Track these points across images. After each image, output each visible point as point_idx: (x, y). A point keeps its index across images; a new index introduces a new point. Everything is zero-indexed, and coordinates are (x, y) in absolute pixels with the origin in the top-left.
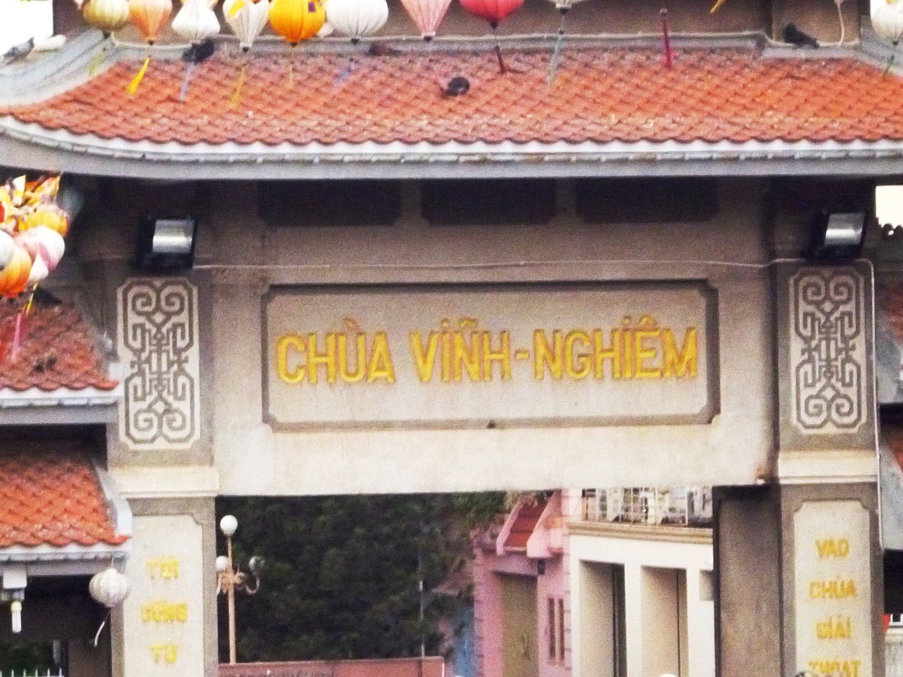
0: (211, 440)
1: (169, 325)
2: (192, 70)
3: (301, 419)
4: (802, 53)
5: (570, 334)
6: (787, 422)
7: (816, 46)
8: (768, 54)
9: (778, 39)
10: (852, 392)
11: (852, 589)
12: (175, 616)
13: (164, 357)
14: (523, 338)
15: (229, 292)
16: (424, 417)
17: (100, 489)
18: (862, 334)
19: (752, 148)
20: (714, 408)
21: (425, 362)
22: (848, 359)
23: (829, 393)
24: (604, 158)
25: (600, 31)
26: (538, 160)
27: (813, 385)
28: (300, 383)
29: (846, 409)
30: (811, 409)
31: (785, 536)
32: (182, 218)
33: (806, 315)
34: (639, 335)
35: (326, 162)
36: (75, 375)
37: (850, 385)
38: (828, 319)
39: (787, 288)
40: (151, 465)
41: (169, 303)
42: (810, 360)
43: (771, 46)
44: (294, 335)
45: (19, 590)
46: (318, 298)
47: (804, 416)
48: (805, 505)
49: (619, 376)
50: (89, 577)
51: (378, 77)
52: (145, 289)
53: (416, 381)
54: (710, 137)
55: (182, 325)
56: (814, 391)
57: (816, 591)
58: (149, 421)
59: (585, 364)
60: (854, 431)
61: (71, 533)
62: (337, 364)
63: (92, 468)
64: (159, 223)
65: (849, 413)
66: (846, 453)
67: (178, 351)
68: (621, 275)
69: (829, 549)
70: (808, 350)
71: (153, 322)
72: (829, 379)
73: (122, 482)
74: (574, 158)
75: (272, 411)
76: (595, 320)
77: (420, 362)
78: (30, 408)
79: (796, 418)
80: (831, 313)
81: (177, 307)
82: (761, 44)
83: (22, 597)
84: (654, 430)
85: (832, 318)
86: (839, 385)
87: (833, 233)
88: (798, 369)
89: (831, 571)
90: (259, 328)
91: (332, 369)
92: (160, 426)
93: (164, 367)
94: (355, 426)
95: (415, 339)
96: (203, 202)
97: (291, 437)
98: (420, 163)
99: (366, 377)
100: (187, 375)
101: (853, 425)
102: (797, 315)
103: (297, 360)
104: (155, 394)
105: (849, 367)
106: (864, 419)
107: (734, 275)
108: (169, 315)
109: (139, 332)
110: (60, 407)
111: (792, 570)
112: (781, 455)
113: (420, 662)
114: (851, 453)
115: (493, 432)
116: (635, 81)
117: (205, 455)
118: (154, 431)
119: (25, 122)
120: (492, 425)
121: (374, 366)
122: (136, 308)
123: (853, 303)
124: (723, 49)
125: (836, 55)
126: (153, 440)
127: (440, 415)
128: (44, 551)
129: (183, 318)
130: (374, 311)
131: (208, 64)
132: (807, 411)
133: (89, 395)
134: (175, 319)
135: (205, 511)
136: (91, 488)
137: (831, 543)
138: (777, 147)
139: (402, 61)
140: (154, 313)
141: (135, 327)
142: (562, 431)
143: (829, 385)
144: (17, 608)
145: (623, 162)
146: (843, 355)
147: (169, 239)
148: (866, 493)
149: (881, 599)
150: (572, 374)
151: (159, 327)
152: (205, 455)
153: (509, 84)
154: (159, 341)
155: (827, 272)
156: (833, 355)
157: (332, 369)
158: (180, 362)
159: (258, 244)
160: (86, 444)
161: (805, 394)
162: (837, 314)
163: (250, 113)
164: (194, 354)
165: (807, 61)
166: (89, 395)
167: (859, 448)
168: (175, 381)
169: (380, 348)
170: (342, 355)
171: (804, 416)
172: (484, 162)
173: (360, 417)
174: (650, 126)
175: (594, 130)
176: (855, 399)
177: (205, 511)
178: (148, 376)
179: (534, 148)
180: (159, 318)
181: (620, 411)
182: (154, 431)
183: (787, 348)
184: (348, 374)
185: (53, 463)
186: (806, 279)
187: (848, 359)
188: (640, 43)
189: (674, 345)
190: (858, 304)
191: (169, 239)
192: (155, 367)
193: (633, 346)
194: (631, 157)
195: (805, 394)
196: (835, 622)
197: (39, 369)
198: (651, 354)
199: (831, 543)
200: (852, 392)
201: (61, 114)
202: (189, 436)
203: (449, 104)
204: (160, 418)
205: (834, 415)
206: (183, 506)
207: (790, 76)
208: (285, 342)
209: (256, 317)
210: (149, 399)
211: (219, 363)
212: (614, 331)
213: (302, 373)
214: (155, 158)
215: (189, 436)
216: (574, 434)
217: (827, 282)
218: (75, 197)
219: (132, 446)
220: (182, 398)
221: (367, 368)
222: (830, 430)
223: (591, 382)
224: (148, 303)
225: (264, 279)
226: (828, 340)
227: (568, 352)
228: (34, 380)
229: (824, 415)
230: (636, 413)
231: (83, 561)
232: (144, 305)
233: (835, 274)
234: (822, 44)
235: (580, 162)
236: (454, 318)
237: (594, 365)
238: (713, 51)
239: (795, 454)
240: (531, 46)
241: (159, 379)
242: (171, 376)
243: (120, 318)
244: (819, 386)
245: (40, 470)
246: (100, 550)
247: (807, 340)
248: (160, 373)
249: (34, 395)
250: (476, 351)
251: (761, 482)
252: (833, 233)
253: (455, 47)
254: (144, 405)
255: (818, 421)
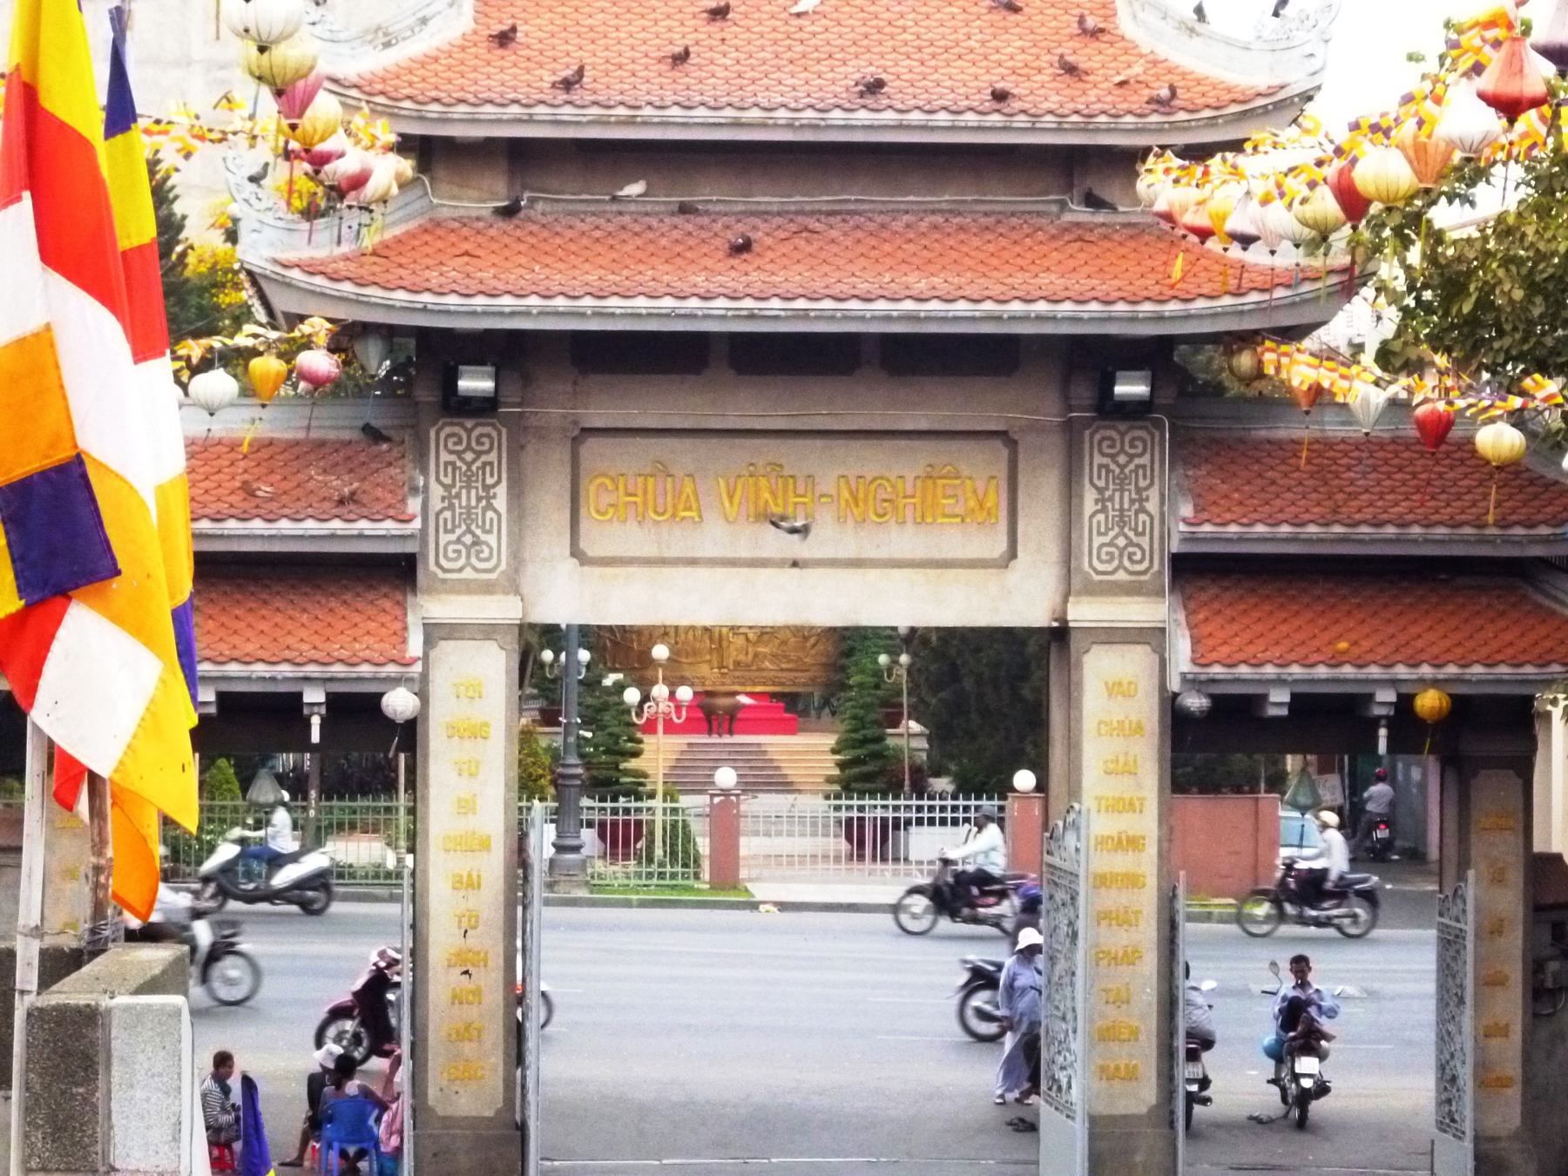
0: (517, 571)
1: (478, 464)
2: (501, 224)
3: (630, 554)
4: (1100, 217)
5: (875, 479)
6: (1080, 569)
7: (1112, 208)
8: (1068, 217)
9: (1079, 204)
10: (1145, 542)
11: (1140, 727)
12: (477, 733)
13: (473, 492)
14: (827, 484)
15: (542, 434)
16: (730, 554)
17: (405, 614)
18: (1156, 486)
19: (1016, 307)
20: (1012, 553)
21: (731, 503)
22: (490, 506)
23: (1121, 542)
24: (868, 315)
25: (907, 195)
26: (804, 315)
27: (1105, 534)
28: (610, 521)
29: (1138, 557)
30: (1104, 557)
31: (1074, 678)
32: (483, 363)
33: (1100, 466)
34: (940, 482)
35: (598, 314)
36: (378, 507)
37: (1143, 534)
38: (469, 469)
39: (1082, 442)
40: (458, 592)
41: (479, 443)
42: (1104, 510)
43: (1071, 210)
44: (604, 475)
45: (319, 704)
46: (629, 440)
47: (1095, 562)
48: (1095, 647)
49: (921, 521)
50: (381, 695)
51: (676, 234)
52: (456, 429)
53: (722, 521)
54: (975, 297)
55: (491, 464)
56: (1106, 539)
57: (1104, 729)
58: (458, 552)
59: (888, 510)
60: (1143, 578)
61: (367, 654)
62: (645, 504)
63: (405, 595)
64: (462, 368)
65: (1141, 562)
66: (1136, 599)
67: (486, 488)
68: (923, 425)
69: (1116, 689)
70: (1101, 500)
71: (462, 460)
72: (1122, 528)
73: (430, 607)
74: (839, 314)
75: (582, 545)
76: (900, 468)
77: (727, 504)
78: (332, 537)
79: (1092, 564)
80: (1126, 466)
81: (486, 447)
82: (1063, 205)
83: (323, 710)
84: (951, 573)
85: (1127, 471)
86: (1131, 534)
87: (1120, 389)
88: (1091, 517)
89: (1119, 711)
90: (569, 469)
91: (640, 509)
92: (468, 557)
93: (473, 503)
94: (663, 562)
95: (722, 482)
96: (511, 350)
97: (597, 571)
98: (691, 316)
99: (674, 516)
100: (496, 511)
101: (1144, 572)
102: (437, 465)
103: (607, 499)
104: (464, 527)
105: (490, 514)
106: (1156, 567)
107: (1035, 428)
108: (479, 454)
109: (450, 469)
110: (361, 536)
111: (1080, 709)
112: (1071, 599)
113: (1257, 799)
114: (1141, 599)
115: (795, 571)
116: (924, 242)
117: (511, 584)
118: (462, 561)
119: (312, 274)
120: (795, 564)
121: (681, 506)
122: (448, 444)
123: (1148, 456)
124: (1023, 213)
125: (1134, 220)
126: (460, 570)
127: (744, 553)
128: (338, 669)
129: (493, 457)
130: (682, 454)
131: (515, 221)
132: (1099, 558)
133: (389, 526)
134: (484, 458)
135: (508, 638)
136: (399, 613)
137: (1120, 684)
138: (1042, 307)
139: (705, 220)
140: (464, 451)
141: (446, 464)
142: (860, 571)
143: (469, 531)
144: (316, 721)
145: (888, 318)
146: (1137, 506)
147: (475, 383)
148: (1154, 637)
149: (1169, 743)
150: (875, 518)
151: (469, 465)
152: (511, 584)
153: (803, 243)
154: (469, 477)
155: (1123, 426)
156: (1126, 506)
157: (640, 509)
158: (488, 498)
159: (569, 388)
160: (397, 572)
161: (1097, 541)
162: (1132, 466)
163: (537, 268)
164: (502, 491)
165: (1103, 224)
166: (389, 526)
167: (1147, 594)
168: (484, 515)
169: (688, 490)
170: (650, 496)
171: (1095, 562)
172: (752, 317)
173: (667, 554)
174: (922, 286)
175: (863, 287)
176: (1147, 548)
177: (508, 638)
178: (458, 511)
179: (748, 303)
180: (469, 456)
181: (920, 554)
182: (462, 561)
183: (1081, 497)
184: (656, 512)
185: (371, 587)
186: (448, 430)
187: (1142, 510)
188: (945, 206)
189: (975, 492)
190: (1152, 455)
191: (475, 383)
192: (464, 503)
193: (934, 495)
194: (895, 314)
195: (1097, 541)
196: (1122, 759)
197: (341, 502)
198: (951, 501)
199: (1120, 684)
200: (1145, 542)
201: (352, 266)
202: (495, 568)
203: (735, 262)
204: (468, 548)
205: (1126, 563)
206: (487, 631)
207: (1080, 239)
208: (599, 480)
209: (567, 457)
210: (458, 532)
211: (530, 500)
212: (917, 478)
213: (611, 511)
214: (436, 308)
215: (495, 568)
216: (873, 574)
217: (1122, 435)
218: (379, 343)
219: (441, 575)
220: (490, 532)
221: (675, 506)
222: (1121, 576)
223: (894, 528)
224: (459, 442)
225: (575, 423)
226: (1122, 491)
227: (871, 496)
228: (335, 511)
229: (1116, 562)
230: (937, 555)
231: (374, 679)
232: (455, 444)
233: (1132, 428)
234: (1121, 209)
235: (845, 318)
236: (761, 463)
237: (896, 508)
238: (1013, 214)
239: (1085, 599)
240: (837, 207)
241: (469, 514)
242: (479, 511)
243: (1087, 459)
244: (1112, 534)
245: (358, 595)
246: (391, 669)
247: (1100, 490)
248: (469, 507)
249: (336, 525)
250: (780, 494)
251: (1055, 624)
252: (1120, 389)
253: (762, 208)
254: (453, 537)
255: (1109, 568)
